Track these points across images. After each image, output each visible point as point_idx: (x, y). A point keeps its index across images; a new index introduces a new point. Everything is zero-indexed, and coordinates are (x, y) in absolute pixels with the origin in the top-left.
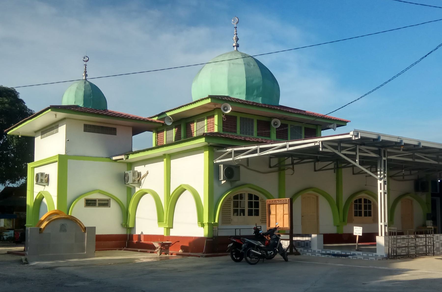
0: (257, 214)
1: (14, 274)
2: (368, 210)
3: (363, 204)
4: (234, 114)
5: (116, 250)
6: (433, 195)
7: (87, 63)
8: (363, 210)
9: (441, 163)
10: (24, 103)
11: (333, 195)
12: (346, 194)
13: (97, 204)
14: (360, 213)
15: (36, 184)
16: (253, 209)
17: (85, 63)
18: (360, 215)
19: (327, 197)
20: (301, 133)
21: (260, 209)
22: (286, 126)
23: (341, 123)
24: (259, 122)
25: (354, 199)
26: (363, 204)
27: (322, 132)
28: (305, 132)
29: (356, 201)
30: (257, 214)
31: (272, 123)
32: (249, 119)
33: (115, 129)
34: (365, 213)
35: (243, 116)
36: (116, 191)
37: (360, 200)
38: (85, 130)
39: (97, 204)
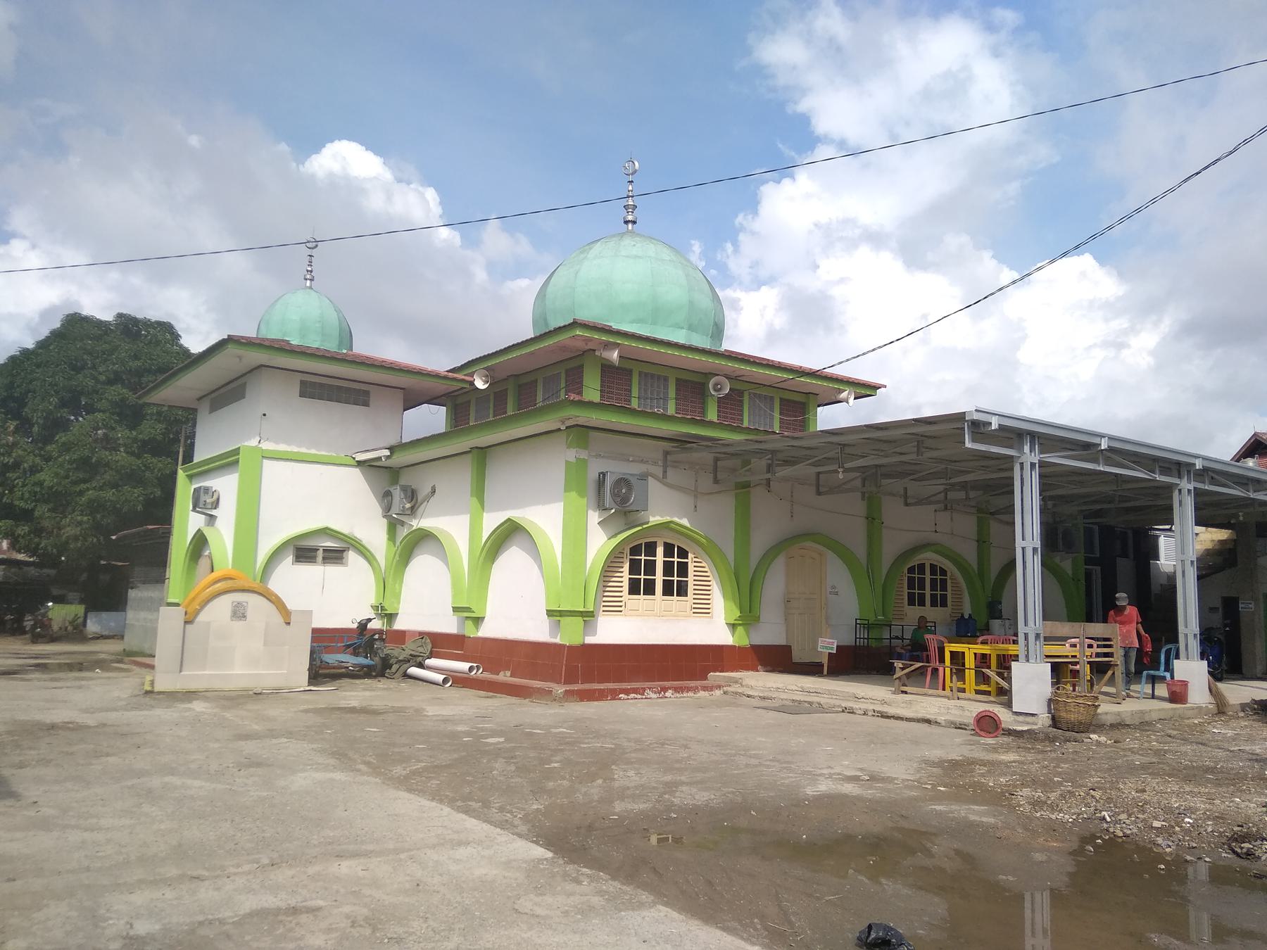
0: (682, 591)
1: (702, 797)
2: (676, 559)
3: (928, 577)
4: (627, 365)
7: (314, 252)
9: (1261, 496)
10: (832, 387)
11: (861, 552)
13: (320, 558)
15: (194, 510)
16: (675, 578)
17: (309, 252)
21: (690, 579)
22: (741, 393)
23: (866, 389)
24: (679, 383)
25: (915, 561)
26: (928, 577)
28: (781, 409)
29: (911, 570)
30: (682, 591)
31: (711, 386)
33: (367, 393)
34: (933, 597)
35: (646, 369)
36: (370, 528)
37: (921, 567)
38: (302, 395)
39: (320, 558)
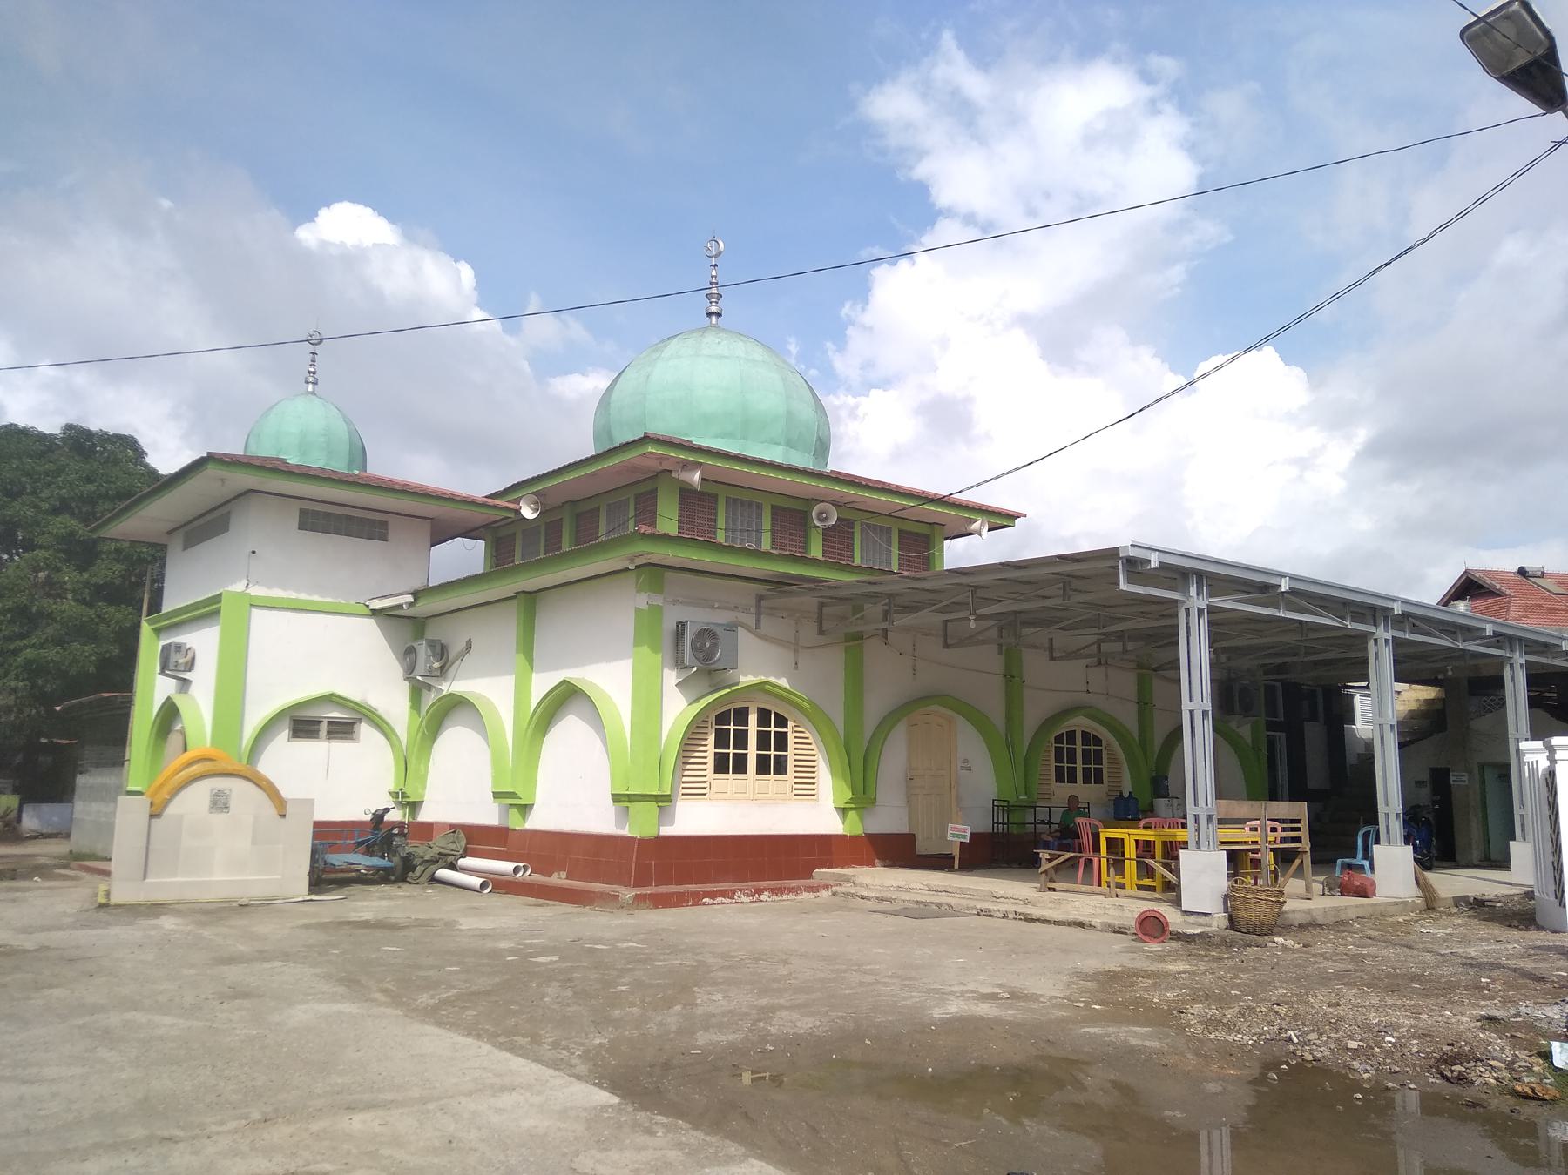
0: (781, 768)
1: (805, 1024)
3: (1079, 747)
5: (729, 894)
6: (1270, 726)
7: (318, 349)
8: (752, 752)
11: (998, 718)
12: (1033, 714)
14: (1072, 771)
15: (162, 672)
16: (772, 753)
17: (311, 348)
18: (740, 767)
19: (979, 721)
20: (889, 544)
23: (1002, 519)
25: (1063, 728)
26: (1079, 747)
27: (946, 543)
29: (1059, 739)
30: (781, 768)
31: (814, 515)
32: (750, 504)
33: (385, 524)
34: (1086, 772)
36: (388, 694)
37: (1071, 736)
38: (302, 526)
